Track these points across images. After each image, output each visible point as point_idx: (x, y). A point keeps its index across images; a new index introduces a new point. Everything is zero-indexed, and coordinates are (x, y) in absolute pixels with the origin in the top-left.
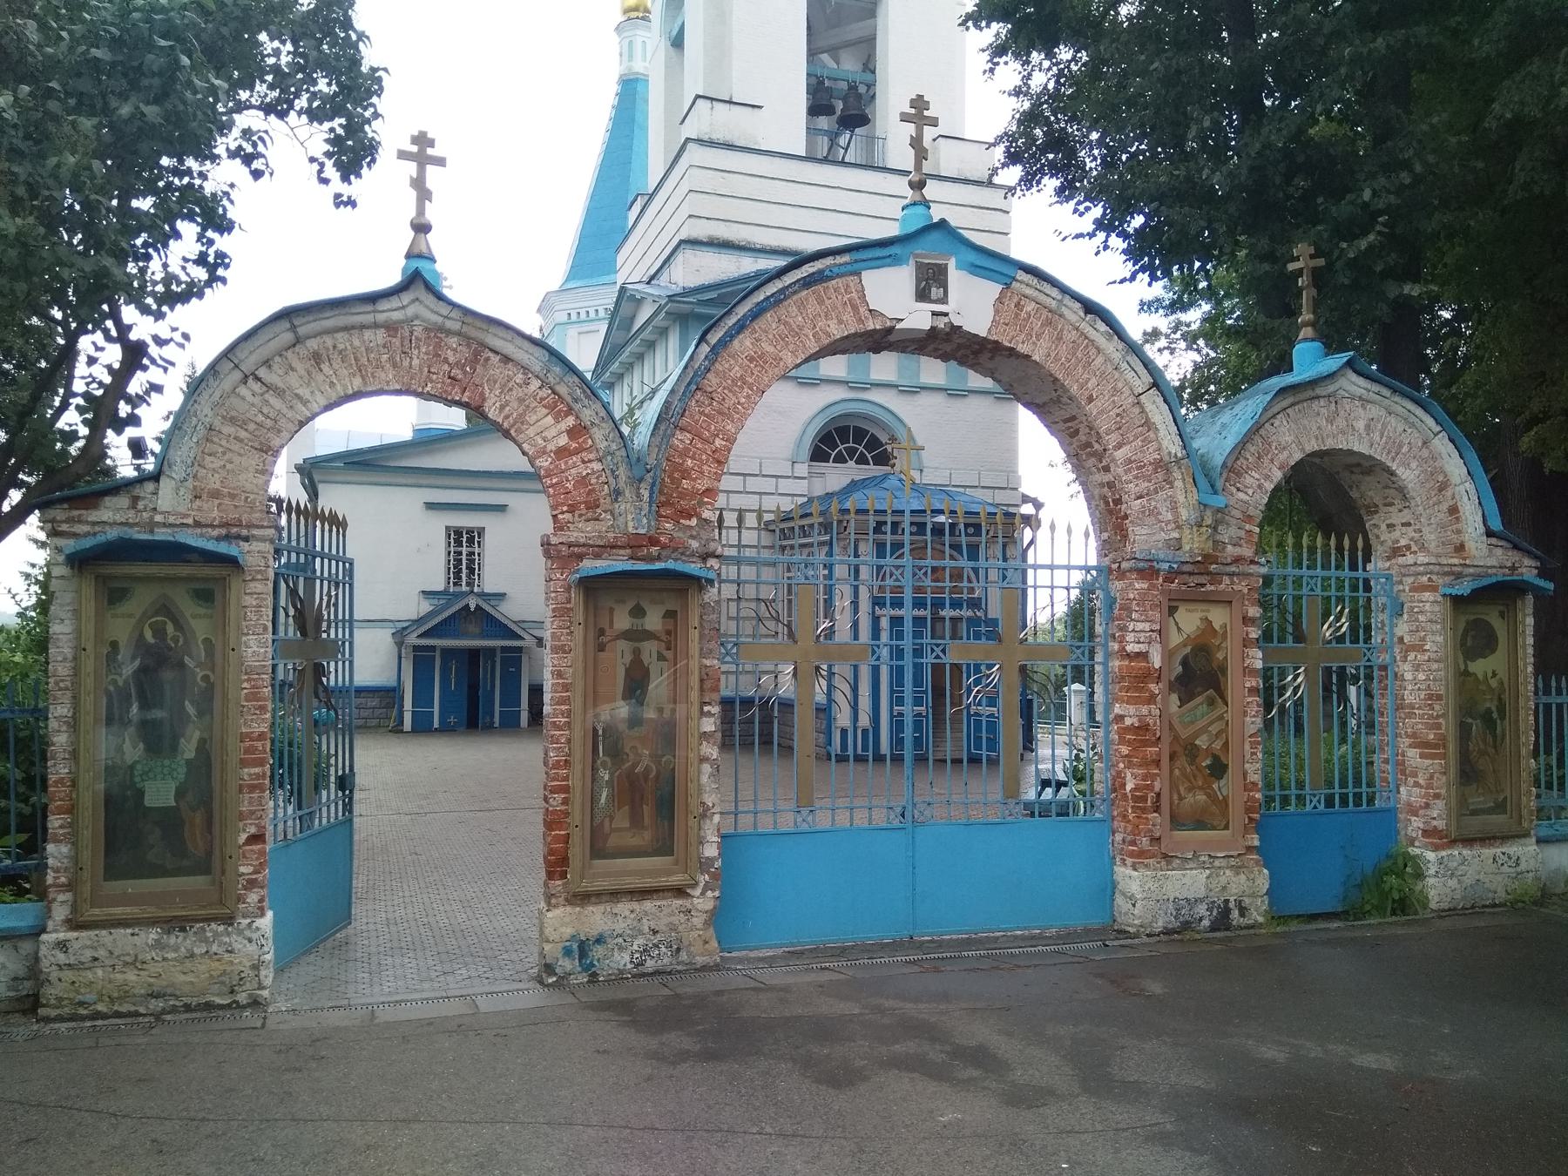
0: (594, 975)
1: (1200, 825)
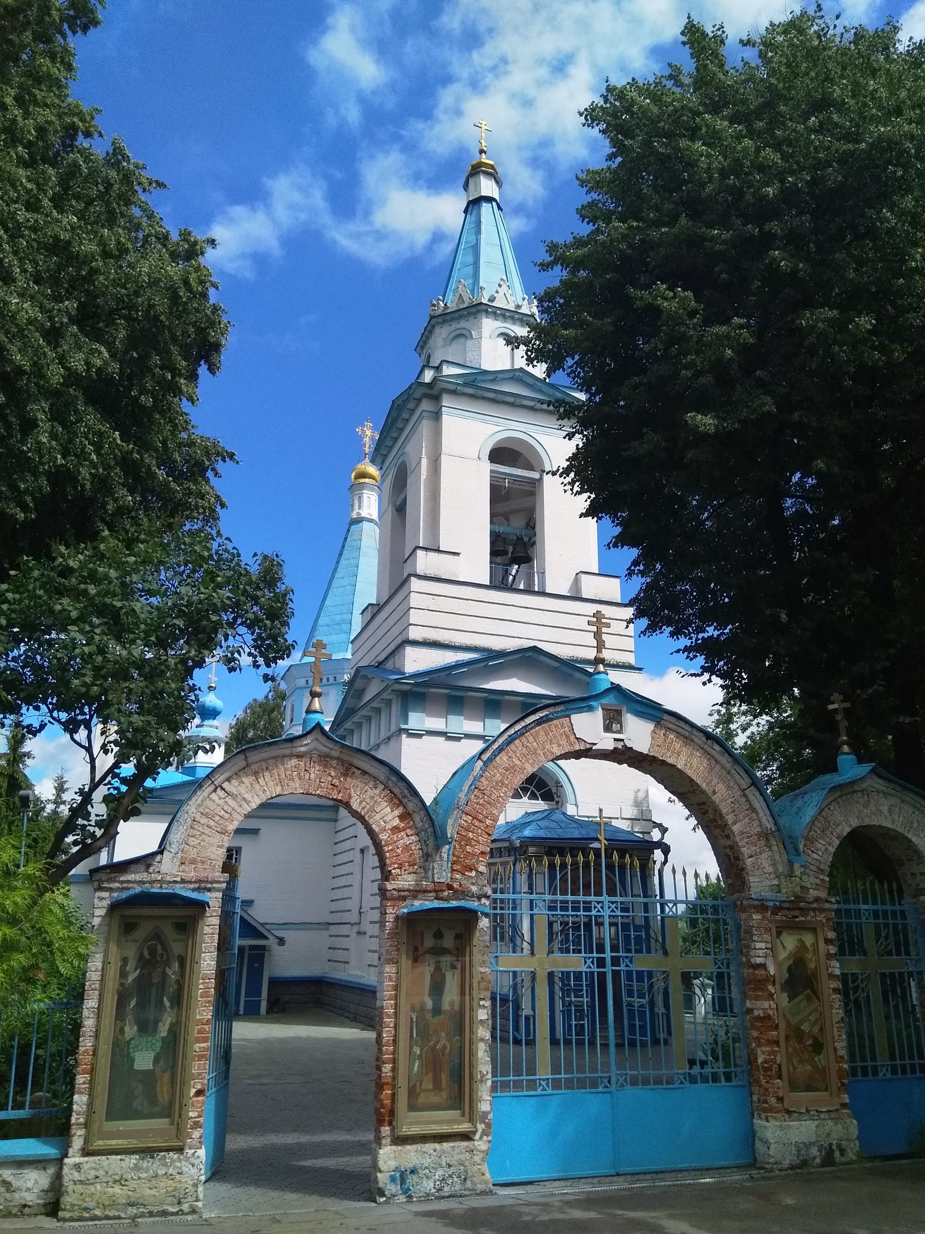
0: (410, 1197)
1: (809, 1088)
